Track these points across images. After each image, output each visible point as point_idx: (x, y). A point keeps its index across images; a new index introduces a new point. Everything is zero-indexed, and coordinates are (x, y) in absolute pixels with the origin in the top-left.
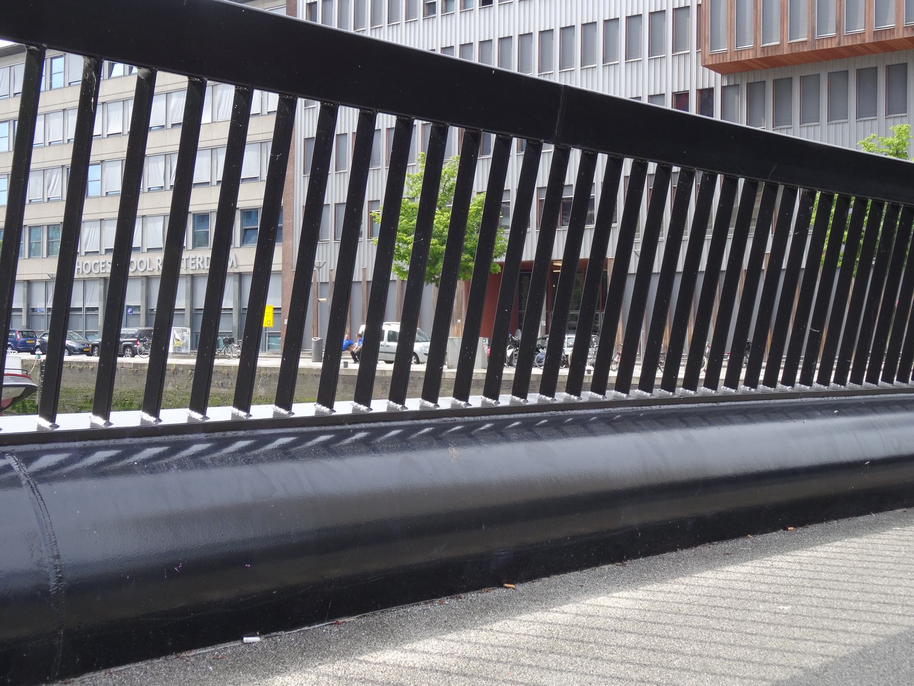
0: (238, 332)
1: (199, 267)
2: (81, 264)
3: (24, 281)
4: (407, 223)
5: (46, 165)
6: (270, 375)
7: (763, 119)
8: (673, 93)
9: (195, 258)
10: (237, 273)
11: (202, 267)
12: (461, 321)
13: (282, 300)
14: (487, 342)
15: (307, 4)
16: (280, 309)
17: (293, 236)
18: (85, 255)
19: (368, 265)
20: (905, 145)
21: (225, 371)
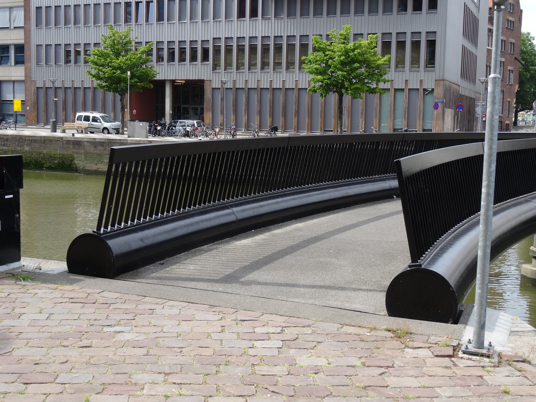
4: (104, 61)
6: (31, 140)
7: (282, 13)
8: (125, 2)
13: (25, 96)
14: (148, 125)
16: (24, 101)
17: (30, 61)
20: (348, 35)
21: (5, 137)
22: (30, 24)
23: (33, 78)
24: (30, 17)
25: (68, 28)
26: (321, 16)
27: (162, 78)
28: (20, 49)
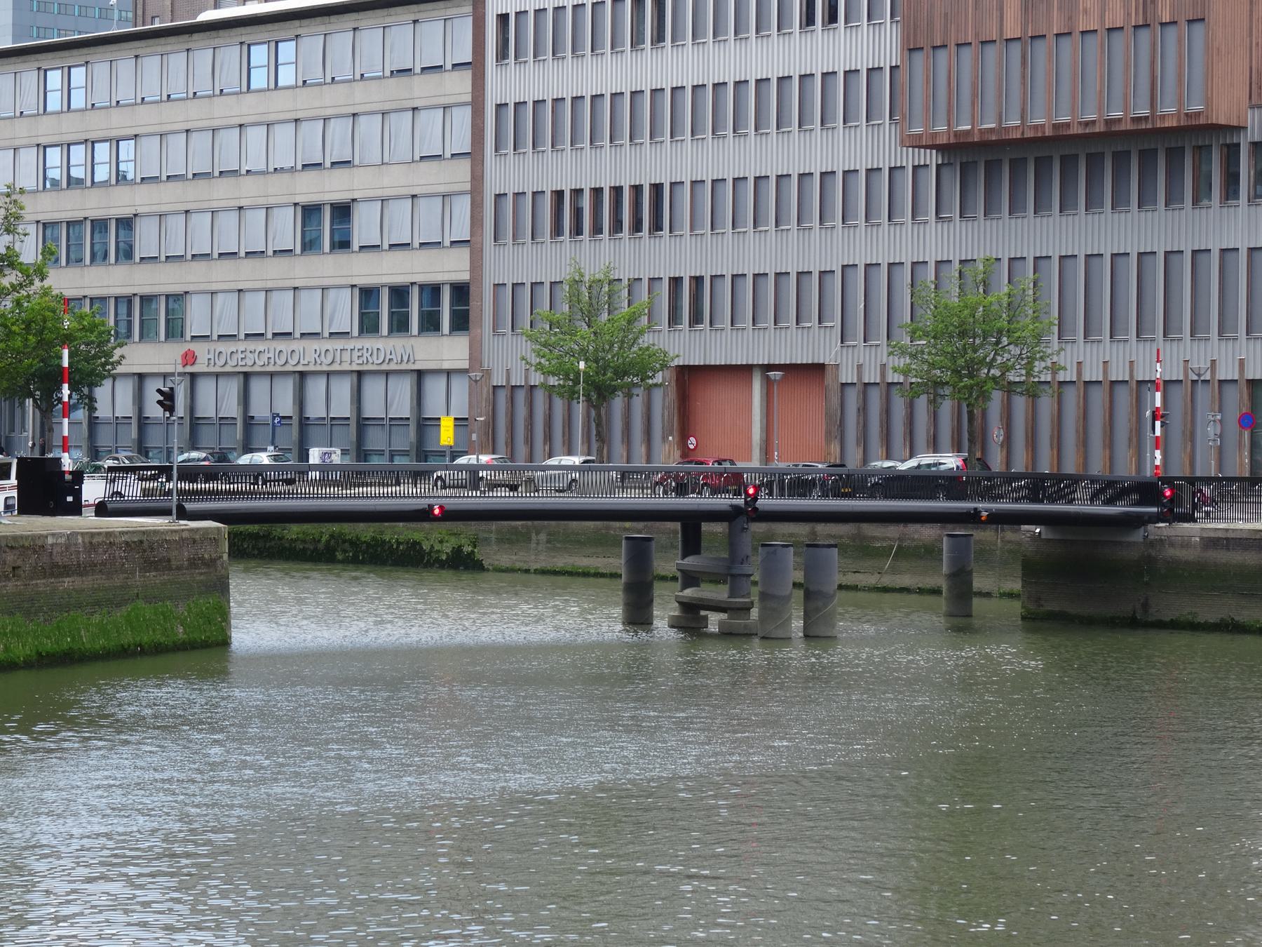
0: (417, 450)
1: (368, 361)
2: (212, 352)
3: (134, 374)
5: (164, 208)
8: (650, 184)
9: (362, 349)
10: (414, 370)
11: (371, 361)
12: (673, 438)
15: (498, 15)
18: (273, 337)
19: (512, 365)
22: (482, 235)
23: (486, 366)
24: (482, 219)
25: (559, 244)
26: (1074, 212)
27: (742, 361)
28: (461, 292)
